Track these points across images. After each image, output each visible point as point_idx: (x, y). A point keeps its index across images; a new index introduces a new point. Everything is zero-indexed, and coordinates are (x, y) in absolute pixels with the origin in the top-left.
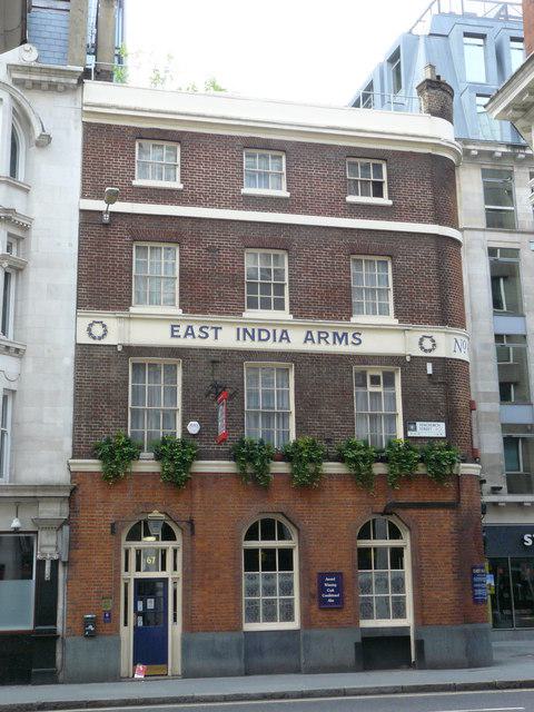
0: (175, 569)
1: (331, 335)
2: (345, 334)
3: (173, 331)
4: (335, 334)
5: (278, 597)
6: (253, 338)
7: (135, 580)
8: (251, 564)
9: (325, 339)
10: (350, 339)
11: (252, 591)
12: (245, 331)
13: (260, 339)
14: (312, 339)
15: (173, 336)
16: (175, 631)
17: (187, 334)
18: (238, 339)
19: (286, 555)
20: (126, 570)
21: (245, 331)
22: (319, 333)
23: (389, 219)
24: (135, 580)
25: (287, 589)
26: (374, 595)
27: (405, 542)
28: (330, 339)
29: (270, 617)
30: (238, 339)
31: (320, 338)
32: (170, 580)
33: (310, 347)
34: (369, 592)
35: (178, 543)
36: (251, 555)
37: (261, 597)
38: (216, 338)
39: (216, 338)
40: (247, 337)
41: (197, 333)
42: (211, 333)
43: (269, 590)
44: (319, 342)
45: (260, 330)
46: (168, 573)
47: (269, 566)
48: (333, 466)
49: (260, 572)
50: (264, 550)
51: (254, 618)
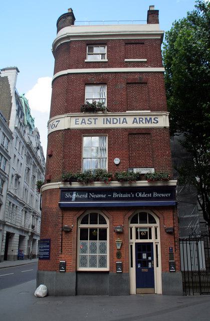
0: (156, 238)
1: (144, 119)
2: (151, 119)
3: (76, 122)
4: (146, 119)
5: (98, 254)
6: (110, 123)
7: (136, 243)
8: (84, 236)
9: (142, 121)
10: (153, 121)
11: (84, 251)
12: (107, 120)
13: (113, 123)
14: (137, 122)
15: (76, 124)
16: (158, 273)
17: (82, 122)
18: (104, 124)
19: (103, 233)
20: (131, 238)
21: (107, 120)
22: (140, 118)
23: (105, 67)
24: (136, 243)
25: (103, 250)
26: (88, 254)
27: (107, 226)
28: (144, 121)
29: (93, 265)
30: (104, 124)
31: (140, 121)
32: (154, 244)
33: (136, 125)
34: (86, 252)
35: (158, 224)
36: (84, 231)
37: (98, 254)
38: (95, 123)
39: (95, 123)
40: (108, 123)
41: (87, 121)
42: (93, 121)
43: (94, 251)
44: (140, 123)
45: (113, 119)
46: (153, 240)
47: (93, 238)
48: (75, 184)
49: (98, 241)
50: (100, 229)
51: (84, 265)
